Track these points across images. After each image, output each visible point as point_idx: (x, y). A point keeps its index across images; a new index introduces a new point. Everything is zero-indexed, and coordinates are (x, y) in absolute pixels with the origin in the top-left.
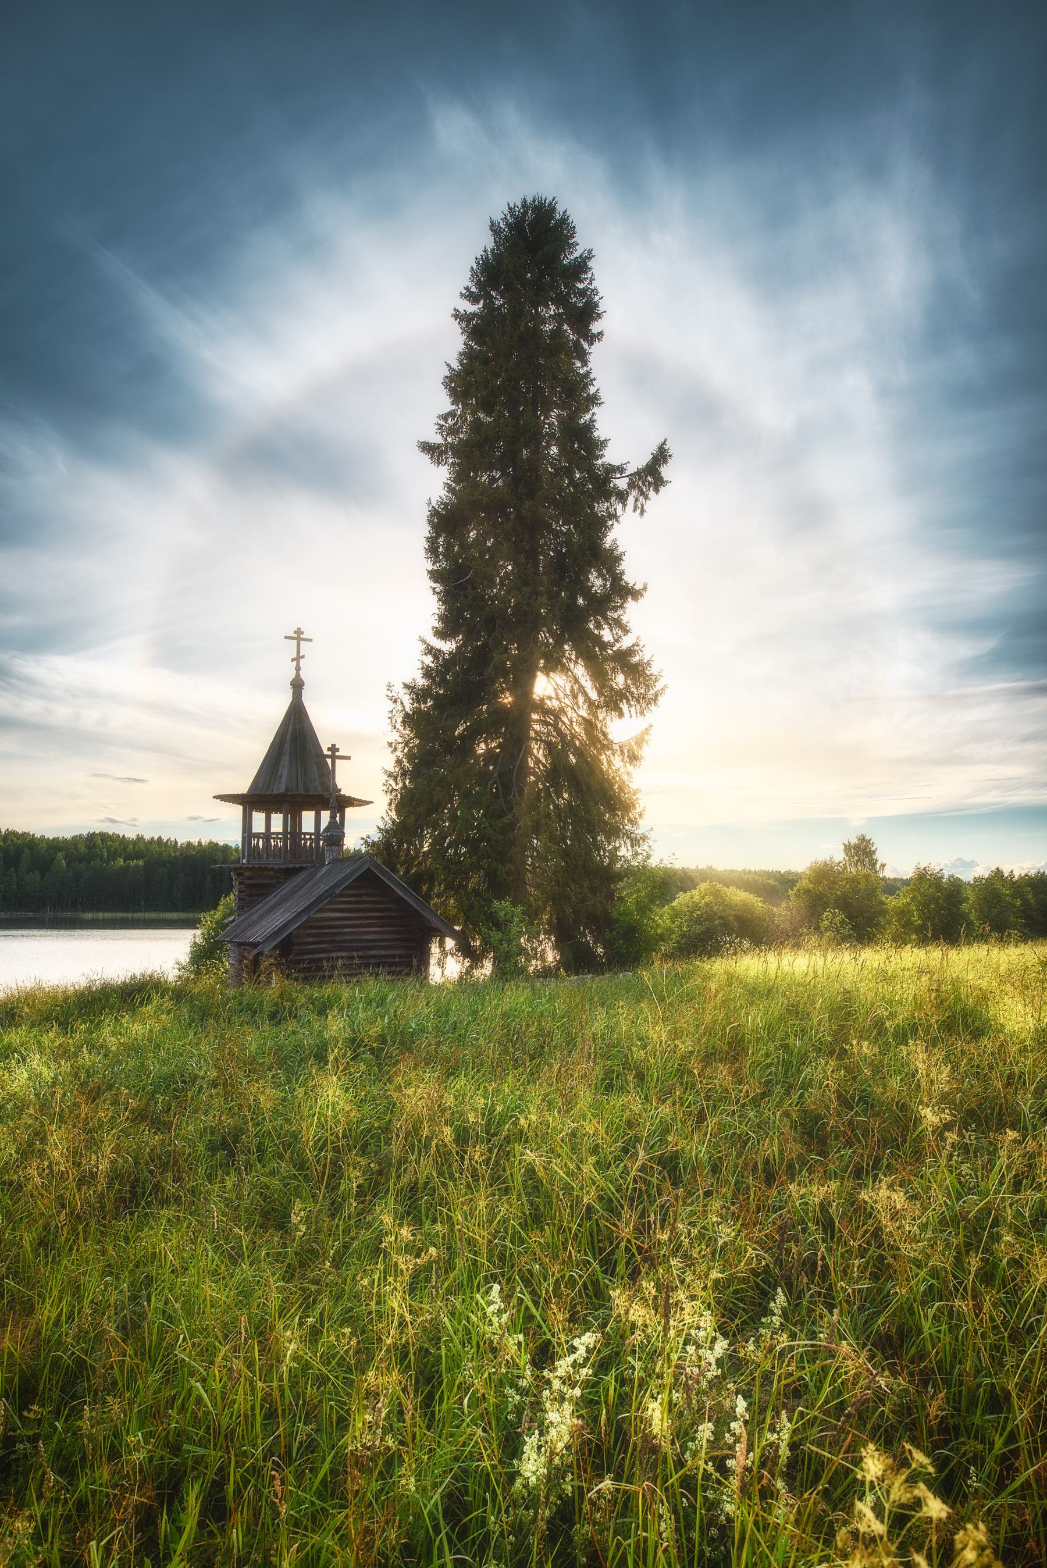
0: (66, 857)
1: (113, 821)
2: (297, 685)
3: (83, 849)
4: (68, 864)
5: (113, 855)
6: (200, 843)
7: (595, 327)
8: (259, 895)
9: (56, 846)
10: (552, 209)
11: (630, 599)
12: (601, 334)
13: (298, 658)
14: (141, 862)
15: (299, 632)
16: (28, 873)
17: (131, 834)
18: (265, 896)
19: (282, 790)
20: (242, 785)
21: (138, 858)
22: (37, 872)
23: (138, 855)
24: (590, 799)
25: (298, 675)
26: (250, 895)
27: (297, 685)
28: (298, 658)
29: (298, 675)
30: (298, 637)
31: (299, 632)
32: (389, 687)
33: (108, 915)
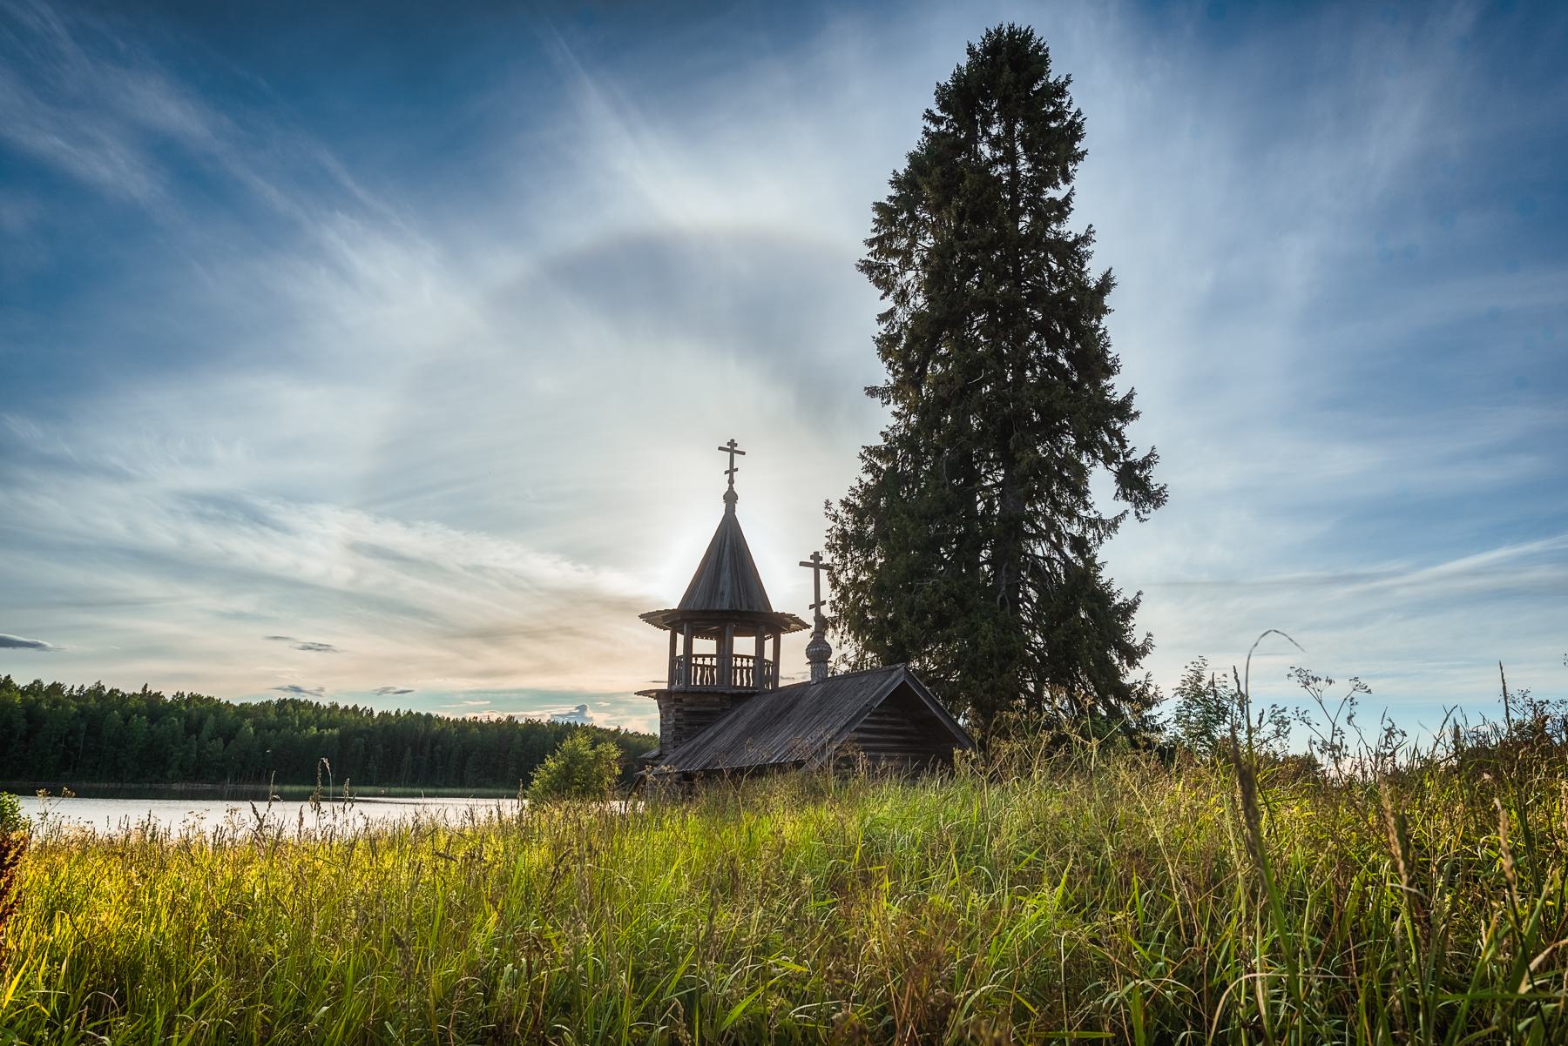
0: (254, 725)
1: (297, 690)
2: (731, 498)
3: (272, 716)
4: (256, 732)
5: (306, 724)
6: (398, 712)
7: (1079, 146)
8: (701, 724)
9: (244, 711)
10: (1028, 37)
11: (376, 715)
12: (1084, 153)
13: (732, 471)
14: (336, 731)
15: (732, 443)
16: (210, 740)
17: (325, 702)
18: (706, 725)
19: (726, 607)
20: (672, 598)
21: (333, 727)
22: (221, 740)
23: (332, 725)
24: (1090, 629)
25: (731, 488)
26: (690, 724)
27: (731, 498)
28: (732, 471)
29: (731, 488)
30: (732, 448)
31: (732, 443)
32: (828, 504)
33: (296, 788)
